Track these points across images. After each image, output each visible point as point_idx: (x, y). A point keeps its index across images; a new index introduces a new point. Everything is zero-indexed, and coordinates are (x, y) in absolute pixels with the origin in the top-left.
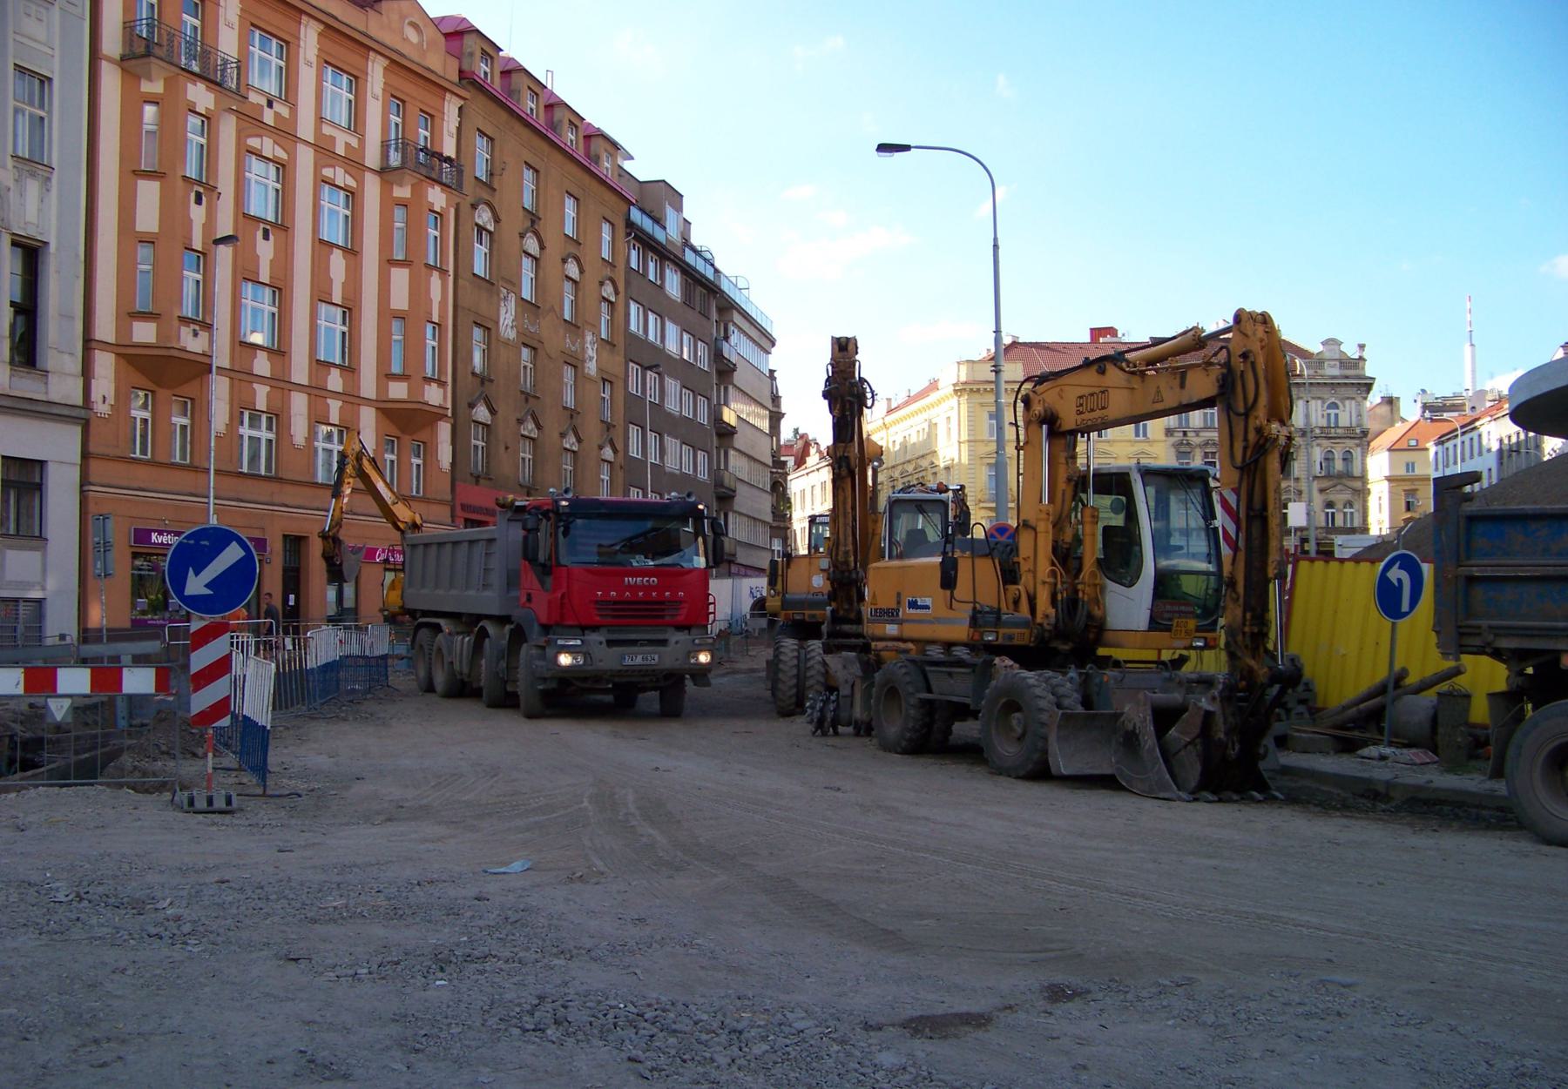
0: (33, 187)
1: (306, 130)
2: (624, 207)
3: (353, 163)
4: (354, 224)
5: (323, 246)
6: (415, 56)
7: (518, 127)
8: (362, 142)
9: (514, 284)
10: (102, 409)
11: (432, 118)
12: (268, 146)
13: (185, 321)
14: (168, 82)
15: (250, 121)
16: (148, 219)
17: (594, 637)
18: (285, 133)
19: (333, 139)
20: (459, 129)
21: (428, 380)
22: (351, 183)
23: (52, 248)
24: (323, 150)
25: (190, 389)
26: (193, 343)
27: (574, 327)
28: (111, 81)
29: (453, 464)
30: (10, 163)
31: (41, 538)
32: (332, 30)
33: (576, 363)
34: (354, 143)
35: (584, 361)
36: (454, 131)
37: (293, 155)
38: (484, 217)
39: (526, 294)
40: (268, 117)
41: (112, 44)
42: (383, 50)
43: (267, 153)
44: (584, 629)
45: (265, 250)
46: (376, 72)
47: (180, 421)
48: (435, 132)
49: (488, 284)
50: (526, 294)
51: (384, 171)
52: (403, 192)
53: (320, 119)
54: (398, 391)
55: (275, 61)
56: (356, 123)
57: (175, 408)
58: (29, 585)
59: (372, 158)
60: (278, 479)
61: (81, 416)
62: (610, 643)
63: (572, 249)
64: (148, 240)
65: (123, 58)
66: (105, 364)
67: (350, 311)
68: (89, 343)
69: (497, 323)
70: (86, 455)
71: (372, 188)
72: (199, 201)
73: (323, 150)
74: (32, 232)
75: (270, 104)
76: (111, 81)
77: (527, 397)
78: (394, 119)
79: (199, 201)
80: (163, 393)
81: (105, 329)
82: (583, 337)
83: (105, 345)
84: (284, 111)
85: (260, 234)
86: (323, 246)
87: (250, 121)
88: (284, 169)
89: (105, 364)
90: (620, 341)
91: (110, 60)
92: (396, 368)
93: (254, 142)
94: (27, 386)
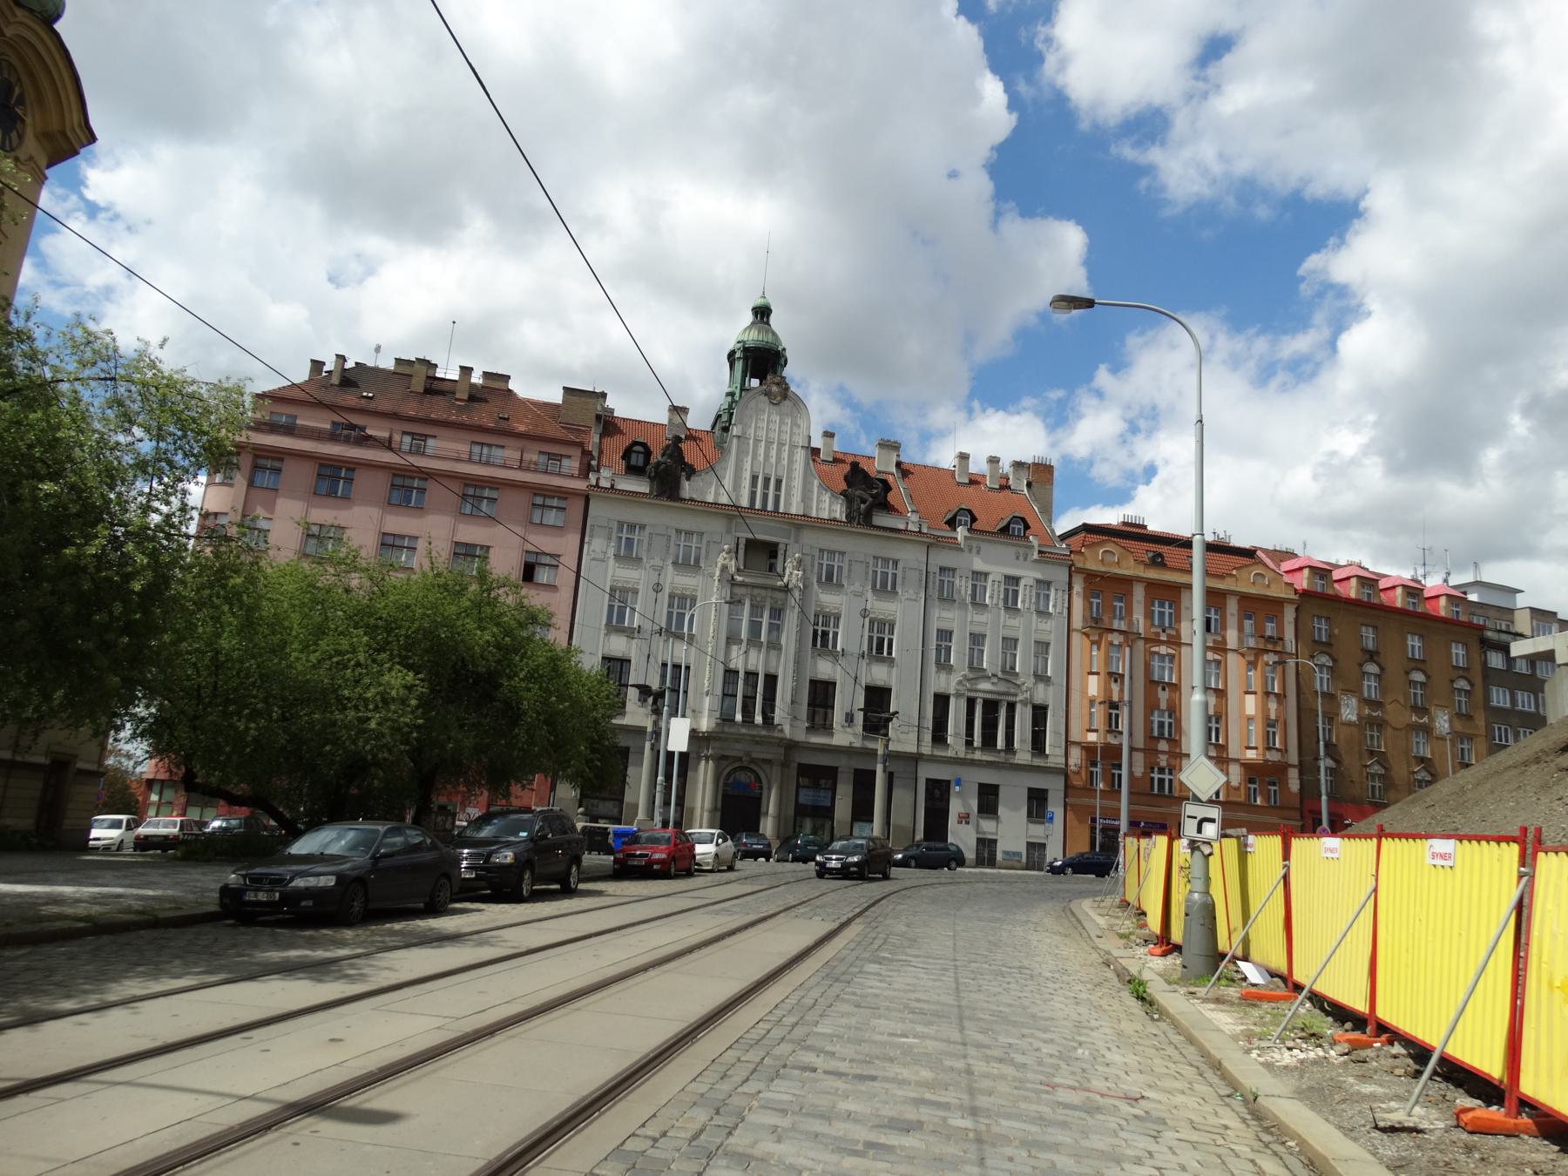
20: (1296, 620)
29: (1301, 789)
55: (1167, 611)
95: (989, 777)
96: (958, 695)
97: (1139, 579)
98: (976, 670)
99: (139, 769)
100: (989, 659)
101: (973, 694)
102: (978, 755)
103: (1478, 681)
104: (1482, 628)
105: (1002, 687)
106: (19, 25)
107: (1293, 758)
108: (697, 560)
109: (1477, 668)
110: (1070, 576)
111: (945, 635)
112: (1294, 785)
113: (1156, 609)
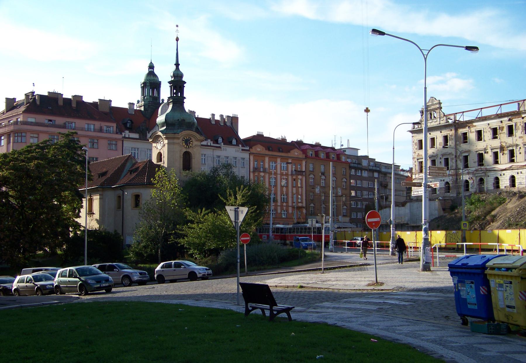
55: (285, 165)
113: (282, 165)
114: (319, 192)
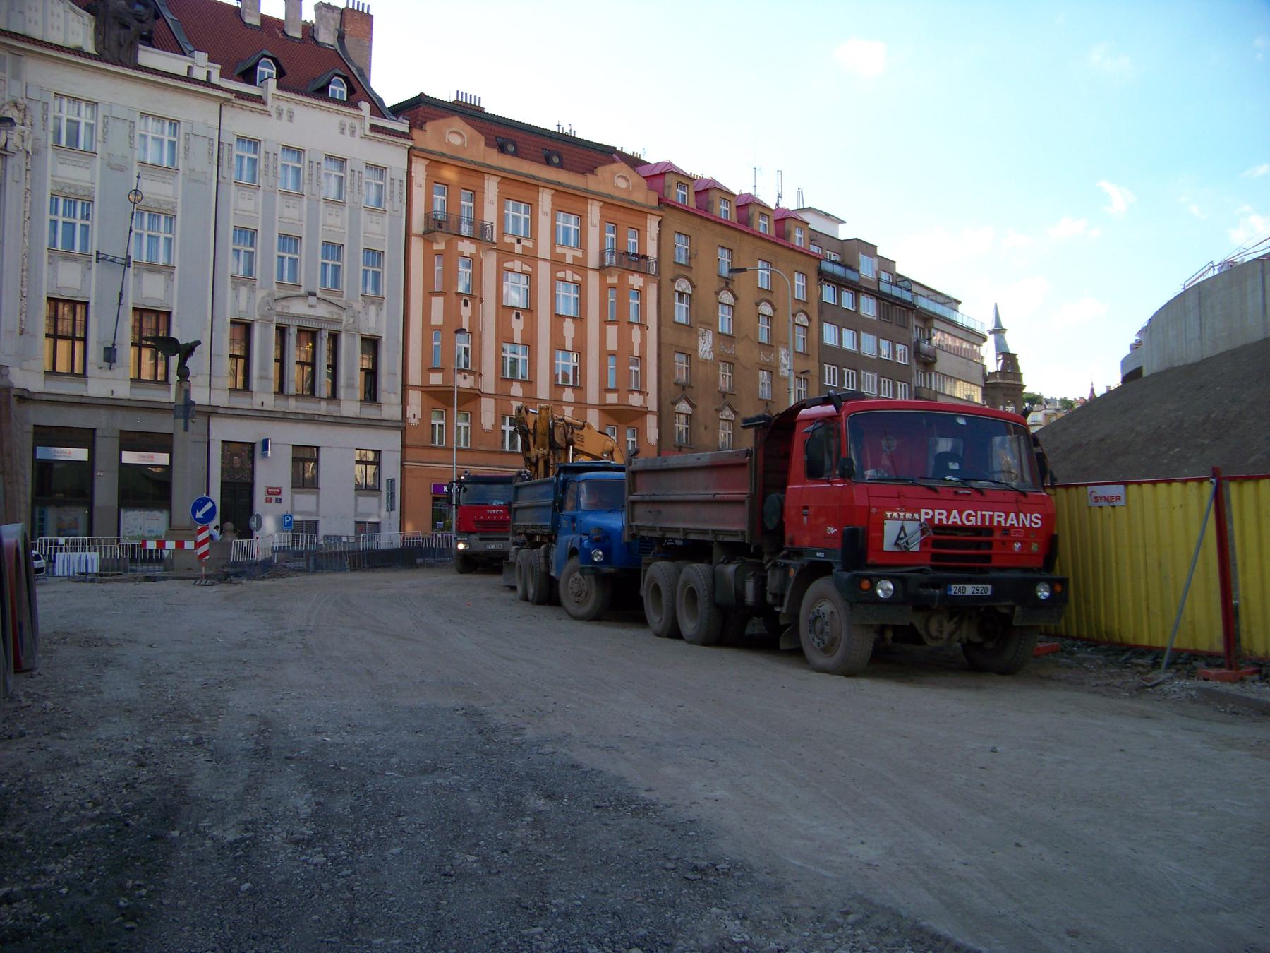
0: (373, 309)
1: (544, 250)
2: (817, 263)
3: (580, 266)
4: (582, 303)
5: (557, 318)
6: (624, 196)
7: (709, 225)
8: (585, 253)
9: (711, 324)
10: (413, 421)
11: (640, 232)
12: (569, 275)
13: (460, 371)
14: (447, 243)
15: (506, 253)
16: (437, 318)
17: (473, 537)
18: (530, 257)
19: (564, 255)
20: (659, 236)
21: (632, 391)
22: (578, 278)
23: (384, 339)
24: (557, 263)
25: (635, 424)
26: (635, 400)
27: (770, 347)
28: (417, 246)
29: (659, 440)
30: (360, 298)
31: (317, 487)
32: (561, 192)
33: (772, 370)
34: (579, 254)
35: (777, 368)
36: (655, 236)
37: (535, 269)
38: (683, 285)
39: (724, 327)
40: (518, 249)
41: (418, 225)
42: (597, 196)
43: (569, 278)
44: (469, 533)
45: (517, 325)
46: (594, 212)
47: (463, 424)
48: (642, 242)
49: (689, 328)
50: (724, 327)
51: (602, 269)
52: (612, 280)
53: (554, 244)
54: (612, 399)
55: (523, 216)
56: (582, 243)
57: (629, 432)
58: (369, 515)
59: (593, 261)
60: (471, 450)
61: (402, 426)
62: (481, 539)
63: (802, 307)
64: (613, 354)
65: (424, 233)
66: (415, 398)
67: (580, 351)
68: (405, 387)
69: (697, 350)
70: (404, 446)
71: (593, 280)
72: (466, 304)
73: (557, 263)
74: (372, 332)
75: (519, 242)
76: (417, 246)
77: (724, 394)
78: (610, 235)
79: (466, 304)
80: (621, 426)
81: (415, 377)
82: (778, 352)
83: (415, 387)
84: (529, 244)
85: (514, 316)
86: (504, 310)
87: (506, 253)
88: (581, 287)
89: (415, 398)
90: (815, 353)
91: (417, 235)
92: (611, 385)
93: (508, 265)
94: (370, 412)
95: (306, 435)
96: (266, 322)
97: (493, 170)
98: (291, 290)
99: (1169, 675)
100: (310, 275)
101: (285, 321)
102: (292, 405)
103: (815, 317)
104: (819, 259)
105: (322, 311)
106: (3, 382)
107: (652, 404)
108: (84, 374)
109: (814, 303)
110: (410, 162)
111: (247, 234)
112: (652, 434)
113: (510, 212)
114: (709, 357)
